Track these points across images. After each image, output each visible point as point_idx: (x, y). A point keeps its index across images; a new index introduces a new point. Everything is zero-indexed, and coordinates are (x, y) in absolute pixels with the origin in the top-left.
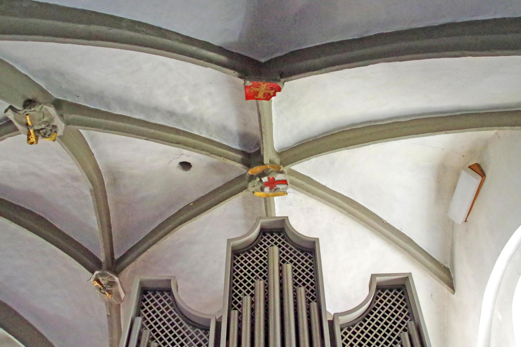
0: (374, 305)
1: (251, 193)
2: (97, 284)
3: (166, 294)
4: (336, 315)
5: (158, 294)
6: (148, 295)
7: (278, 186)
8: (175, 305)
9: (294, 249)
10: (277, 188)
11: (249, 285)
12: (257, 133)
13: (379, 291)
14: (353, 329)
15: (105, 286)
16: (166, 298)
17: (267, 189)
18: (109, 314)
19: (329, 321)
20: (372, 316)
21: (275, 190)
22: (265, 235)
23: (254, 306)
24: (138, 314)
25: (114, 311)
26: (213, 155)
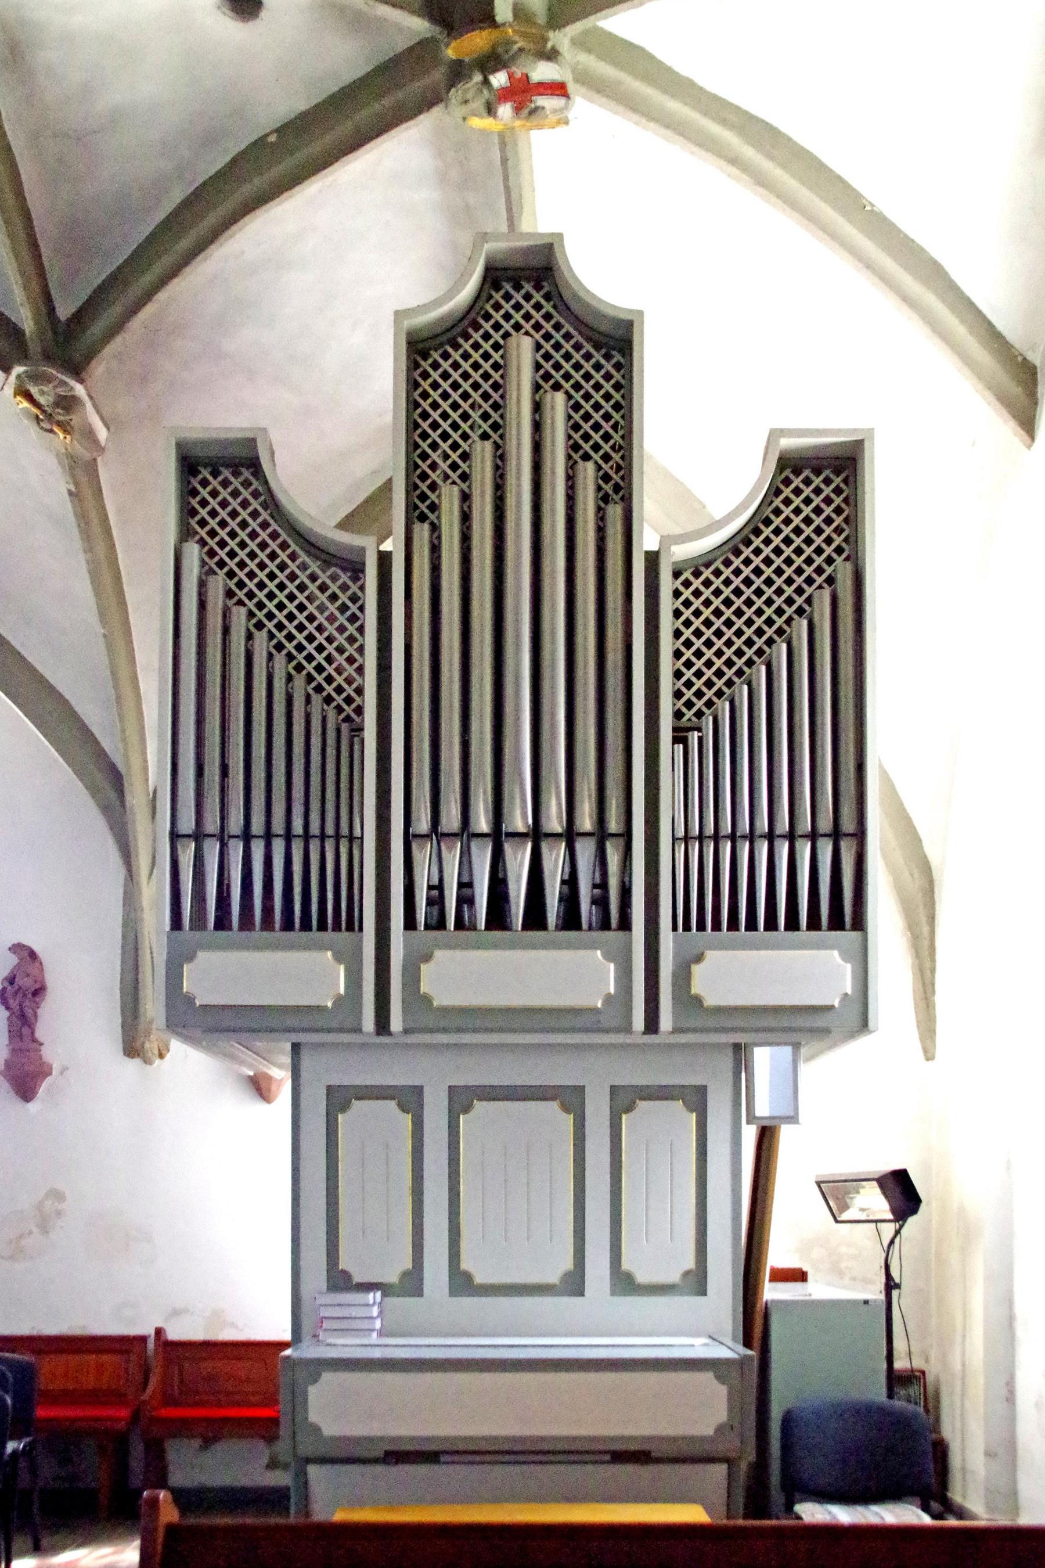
0: (768, 512)
1: (460, 120)
2: (25, 404)
3: (246, 474)
4: (667, 540)
5: (226, 473)
6: (200, 477)
7: (541, 101)
8: (272, 507)
9: (577, 337)
11: (455, 447)
13: (787, 473)
14: (707, 573)
15: (49, 410)
16: (247, 484)
17: (505, 110)
18: (72, 488)
19: (647, 553)
20: (757, 542)
21: (533, 112)
22: (497, 287)
23: (469, 507)
24: (185, 533)
25: (84, 479)
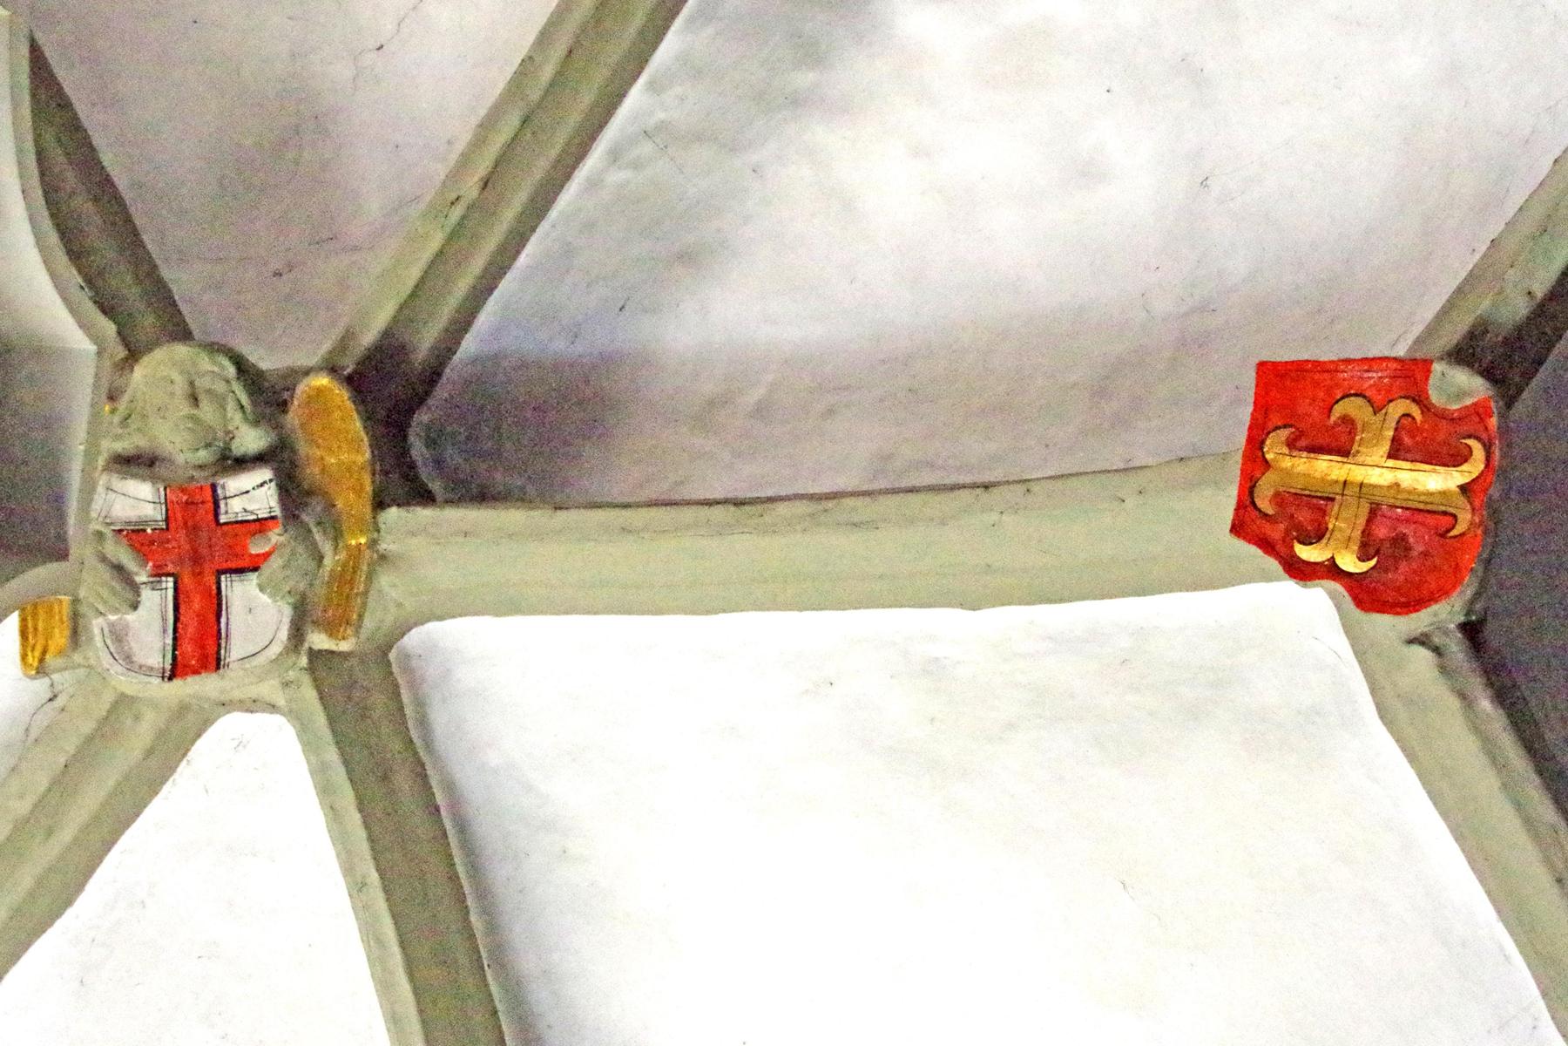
7: (156, 602)
10: (135, 588)
12: (623, 478)
26: (512, 121)
